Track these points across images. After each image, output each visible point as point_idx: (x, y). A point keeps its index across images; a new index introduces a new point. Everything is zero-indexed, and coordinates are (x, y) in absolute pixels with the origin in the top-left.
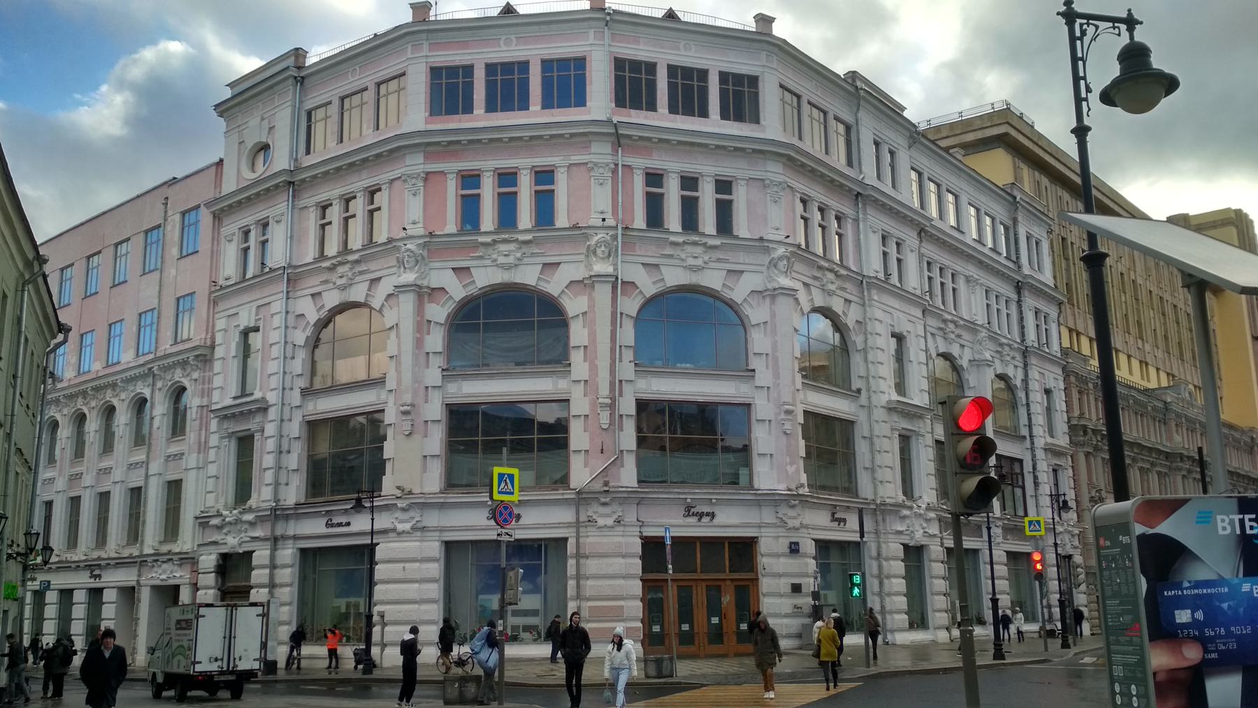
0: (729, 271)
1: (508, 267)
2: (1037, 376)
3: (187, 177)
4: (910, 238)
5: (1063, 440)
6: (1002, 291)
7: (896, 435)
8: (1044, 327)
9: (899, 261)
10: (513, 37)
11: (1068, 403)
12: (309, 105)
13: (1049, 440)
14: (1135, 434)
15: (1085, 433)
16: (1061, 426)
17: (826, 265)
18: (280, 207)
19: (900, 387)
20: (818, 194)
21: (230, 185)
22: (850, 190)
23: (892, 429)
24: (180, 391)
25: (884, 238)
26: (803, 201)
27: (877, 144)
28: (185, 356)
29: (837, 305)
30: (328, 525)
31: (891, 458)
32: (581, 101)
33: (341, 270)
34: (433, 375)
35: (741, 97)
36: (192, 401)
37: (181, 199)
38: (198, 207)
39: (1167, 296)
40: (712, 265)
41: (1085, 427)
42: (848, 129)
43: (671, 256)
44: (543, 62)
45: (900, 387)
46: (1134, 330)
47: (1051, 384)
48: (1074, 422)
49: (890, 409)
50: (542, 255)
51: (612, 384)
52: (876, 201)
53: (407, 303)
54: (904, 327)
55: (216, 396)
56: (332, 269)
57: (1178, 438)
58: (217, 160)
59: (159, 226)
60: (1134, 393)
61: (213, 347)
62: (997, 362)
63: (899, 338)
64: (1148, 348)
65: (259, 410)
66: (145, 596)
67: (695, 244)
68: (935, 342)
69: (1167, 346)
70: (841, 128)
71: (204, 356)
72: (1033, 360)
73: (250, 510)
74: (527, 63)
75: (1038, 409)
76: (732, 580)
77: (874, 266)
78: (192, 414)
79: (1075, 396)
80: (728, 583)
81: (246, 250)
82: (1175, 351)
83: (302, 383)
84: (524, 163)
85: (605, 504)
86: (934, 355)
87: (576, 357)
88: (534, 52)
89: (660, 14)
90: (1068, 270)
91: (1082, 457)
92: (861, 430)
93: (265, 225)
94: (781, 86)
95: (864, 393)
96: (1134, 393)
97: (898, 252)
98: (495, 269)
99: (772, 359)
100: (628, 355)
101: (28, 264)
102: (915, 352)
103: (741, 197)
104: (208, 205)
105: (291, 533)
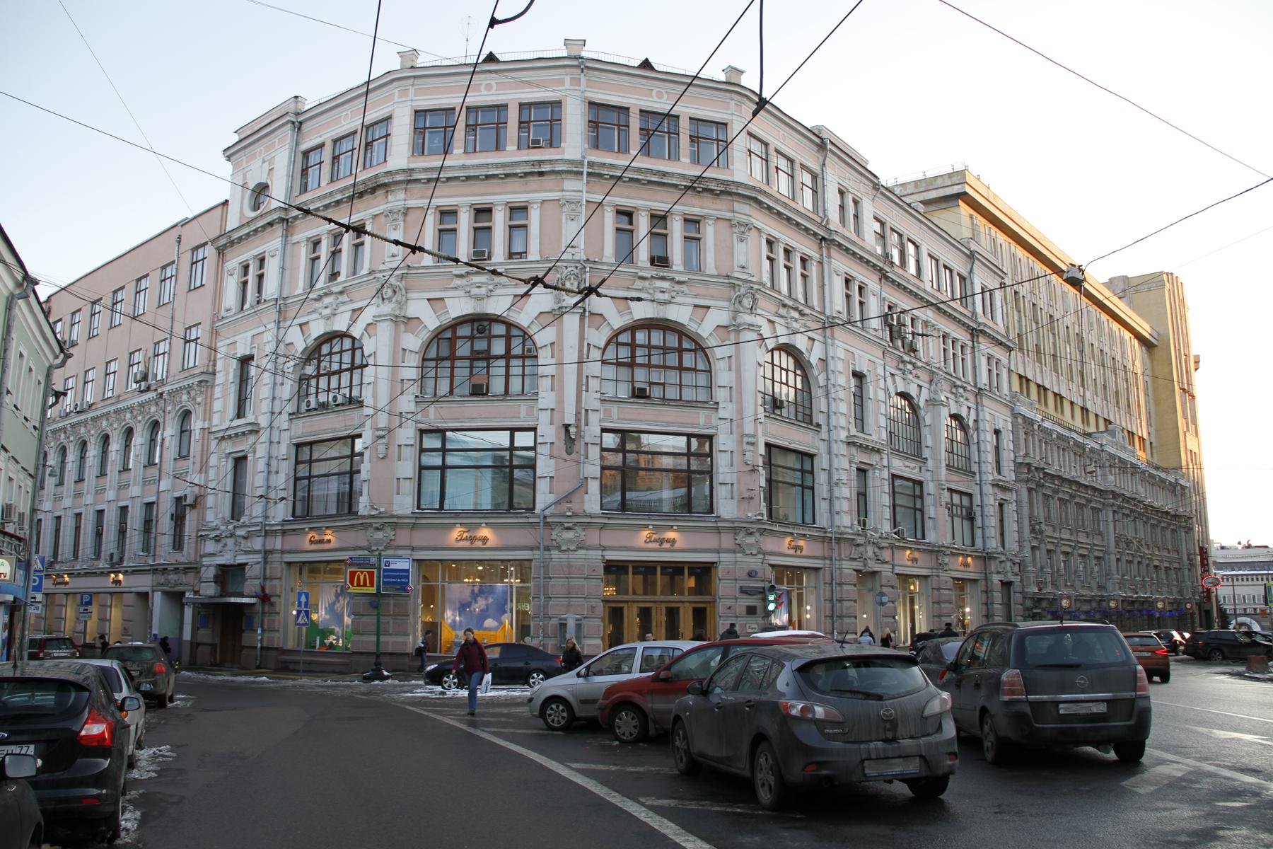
0: (696, 306)
2: (988, 417)
3: (195, 218)
4: (872, 283)
5: (1009, 475)
6: (957, 336)
7: (854, 467)
8: (995, 372)
9: (861, 303)
11: (1015, 442)
12: (305, 146)
13: (997, 477)
14: (1073, 473)
15: (1029, 471)
16: (1008, 466)
17: (791, 303)
18: (272, 243)
19: (860, 421)
20: (787, 237)
21: (232, 223)
22: (815, 234)
23: (850, 462)
24: (186, 414)
25: (847, 281)
26: (770, 243)
27: (841, 193)
28: (190, 382)
29: (801, 342)
31: (846, 492)
32: (553, 142)
33: (327, 300)
34: (406, 403)
35: (708, 135)
36: (196, 424)
37: (193, 236)
38: (206, 243)
39: (1106, 350)
41: (1029, 465)
42: (814, 177)
45: (860, 421)
46: (1077, 378)
47: (1000, 426)
48: (1020, 460)
49: (849, 443)
51: (578, 413)
52: (840, 245)
53: (385, 332)
54: (863, 367)
55: (216, 419)
56: (319, 299)
57: (1111, 478)
58: (223, 200)
59: (173, 262)
60: (1074, 435)
61: (214, 374)
62: (952, 402)
64: (1088, 395)
65: (251, 432)
66: (157, 598)
67: (663, 278)
68: (894, 382)
69: (1106, 394)
70: (807, 179)
71: (207, 380)
72: (986, 401)
73: (244, 526)
74: (506, 106)
75: (989, 447)
77: (837, 303)
78: (196, 435)
79: (1022, 436)
80: (687, 605)
81: (245, 283)
82: (1113, 400)
83: (291, 408)
84: (499, 197)
85: (569, 528)
86: (893, 394)
87: (545, 384)
88: (512, 95)
89: (637, 64)
90: (1020, 321)
91: (1025, 493)
92: (822, 462)
93: (262, 260)
95: (824, 428)
96: (1074, 435)
97: (860, 295)
98: (468, 300)
99: (736, 391)
101: (19, 285)
102: (874, 391)
104: (214, 241)
105: (278, 546)
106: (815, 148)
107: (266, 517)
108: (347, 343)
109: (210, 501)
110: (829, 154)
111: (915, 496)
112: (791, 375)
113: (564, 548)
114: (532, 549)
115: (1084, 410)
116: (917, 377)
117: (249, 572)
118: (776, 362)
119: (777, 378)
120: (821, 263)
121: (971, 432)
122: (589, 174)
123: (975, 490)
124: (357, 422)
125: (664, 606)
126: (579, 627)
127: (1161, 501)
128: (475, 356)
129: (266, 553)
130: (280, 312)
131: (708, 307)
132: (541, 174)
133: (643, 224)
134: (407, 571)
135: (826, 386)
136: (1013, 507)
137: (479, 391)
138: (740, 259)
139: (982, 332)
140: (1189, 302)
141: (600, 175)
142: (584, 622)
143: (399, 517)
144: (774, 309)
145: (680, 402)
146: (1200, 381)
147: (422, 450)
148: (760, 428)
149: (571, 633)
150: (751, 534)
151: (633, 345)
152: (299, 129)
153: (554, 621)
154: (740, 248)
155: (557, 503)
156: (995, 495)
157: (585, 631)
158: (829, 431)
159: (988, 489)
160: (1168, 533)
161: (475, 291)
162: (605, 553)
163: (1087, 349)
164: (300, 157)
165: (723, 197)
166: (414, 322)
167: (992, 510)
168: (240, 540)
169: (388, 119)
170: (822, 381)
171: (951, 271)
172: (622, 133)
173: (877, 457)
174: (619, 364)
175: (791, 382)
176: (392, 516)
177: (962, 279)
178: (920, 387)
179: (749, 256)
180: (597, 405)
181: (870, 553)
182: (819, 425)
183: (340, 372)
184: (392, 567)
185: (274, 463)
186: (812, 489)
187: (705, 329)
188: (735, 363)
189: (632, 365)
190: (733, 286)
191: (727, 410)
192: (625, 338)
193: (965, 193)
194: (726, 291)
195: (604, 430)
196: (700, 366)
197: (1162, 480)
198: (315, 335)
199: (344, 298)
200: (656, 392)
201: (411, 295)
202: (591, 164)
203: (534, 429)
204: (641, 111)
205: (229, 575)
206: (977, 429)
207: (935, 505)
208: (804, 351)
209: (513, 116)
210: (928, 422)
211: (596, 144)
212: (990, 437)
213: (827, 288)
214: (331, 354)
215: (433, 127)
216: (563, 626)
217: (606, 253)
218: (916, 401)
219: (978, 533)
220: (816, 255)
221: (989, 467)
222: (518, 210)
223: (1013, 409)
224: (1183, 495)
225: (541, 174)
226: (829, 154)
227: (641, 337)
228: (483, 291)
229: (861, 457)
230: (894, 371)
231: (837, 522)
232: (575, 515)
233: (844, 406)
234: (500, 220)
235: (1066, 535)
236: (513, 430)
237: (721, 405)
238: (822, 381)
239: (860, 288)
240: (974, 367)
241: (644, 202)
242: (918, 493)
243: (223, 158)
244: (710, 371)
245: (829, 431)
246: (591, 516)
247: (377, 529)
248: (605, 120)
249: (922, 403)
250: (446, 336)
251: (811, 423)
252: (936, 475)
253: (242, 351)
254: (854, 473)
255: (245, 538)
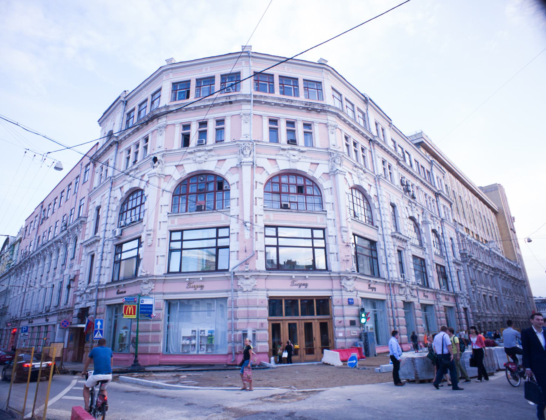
1: (200, 163)
7: (396, 248)
10: (208, 67)
16: (458, 255)
20: (354, 136)
22: (367, 137)
23: (394, 245)
27: (376, 124)
29: (366, 187)
30: (118, 293)
31: (394, 260)
40: (302, 160)
42: (364, 115)
43: (282, 155)
44: (222, 76)
47: (452, 236)
48: (462, 252)
49: (392, 236)
50: (219, 155)
51: (251, 217)
52: (378, 144)
54: (395, 202)
61: (87, 218)
63: (393, 206)
67: (294, 150)
76: (318, 319)
80: (316, 321)
84: (211, 116)
85: (247, 279)
87: (233, 203)
94: (333, 89)
95: (380, 228)
100: (260, 202)
103: (317, 130)
105: (104, 297)
106: (363, 102)
107: (99, 282)
108: (140, 194)
109: (80, 277)
110: (369, 105)
111: (422, 266)
112: (362, 202)
113: (245, 290)
114: (227, 291)
115: (477, 235)
116: (417, 210)
117: (90, 311)
118: (354, 194)
119: (355, 202)
120: (371, 152)
121: (441, 238)
122: (254, 101)
123: (446, 265)
124: (140, 230)
125: (303, 322)
126: (254, 335)
127: (513, 274)
128: (199, 192)
129: (98, 301)
130: (112, 183)
131: (318, 164)
132: (231, 103)
133: (283, 127)
134: (152, 305)
135: (379, 208)
136: (462, 273)
137: (199, 209)
138: (332, 142)
139: (440, 194)
140: (507, 196)
141: (260, 102)
142: (257, 333)
143: (156, 276)
144: (352, 168)
145: (307, 212)
146: (516, 225)
147: (171, 241)
148: (349, 225)
149: (250, 337)
150: (349, 280)
151: (280, 184)
152: (126, 104)
153: (240, 333)
154: (332, 137)
155: (241, 264)
156: (455, 267)
157: (258, 338)
158: (383, 230)
159: (452, 264)
160: (518, 287)
161: (198, 159)
162: (269, 292)
163: (474, 211)
164: (126, 116)
165: (321, 113)
166: (169, 178)
167: (454, 274)
168: (88, 295)
169: (160, 90)
170: (377, 206)
171: (424, 168)
172: (271, 87)
173: (405, 244)
174: (273, 193)
175: (362, 205)
176: (153, 276)
177: (428, 172)
178: (419, 215)
179: (337, 140)
180: (262, 212)
181: (408, 292)
182: (377, 227)
183: (135, 208)
184: (145, 303)
185: (105, 255)
186: (377, 259)
187: (317, 174)
188: (334, 190)
189: (280, 193)
190: (330, 154)
191: (331, 214)
192: (276, 180)
193: (423, 142)
194: (327, 157)
195: (266, 226)
196: (316, 193)
197: (512, 265)
198: (125, 191)
199: (138, 171)
200: (293, 207)
201: (167, 164)
202: (255, 96)
203: (228, 227)
204: (280, 76)
205: (84, 313)
206: (443, 237)
207: (432, 270)
208: (367, 190)
209: (218, 80)
210: (424, 231)
211: (257, 90)
212: (449, 241)
213: (374, 162)
214: (133, 200)
215: (181, 89)
216: (245, 335)
217: (264, 138)
218: (417, 221)
219: (450, 285)
220: (368, 148)
221: (450, 254)
222: (220, 122)
223: (456, 230)
224: (520, 272)
225: (231, 103)
226: (369, 105)
227: (284, 180)
228: (203, 159)
229: (398, 243)
230: (407, 206)
231: (391, 276)
232: (250, 271)
233: (388, 218)
234: (211, 128)
235: (483, 287)
236: (218, 228)
237: (328, 212)
238: (377, 206)
239: (389, 167)
240: (438, 210)
241: (283, 115)
242: (423, 264)
243: (97, 124)
244: (321, 196)
245: (383, 230)
246: (259, 271)
247: (145, 283)
248: (262, 80)
249: (420, 223)
250: (184, 183)
251: (373, 225)
252: (432, 255)
253: (97, 204)
254: (397, 252)
255: (90, 293)
